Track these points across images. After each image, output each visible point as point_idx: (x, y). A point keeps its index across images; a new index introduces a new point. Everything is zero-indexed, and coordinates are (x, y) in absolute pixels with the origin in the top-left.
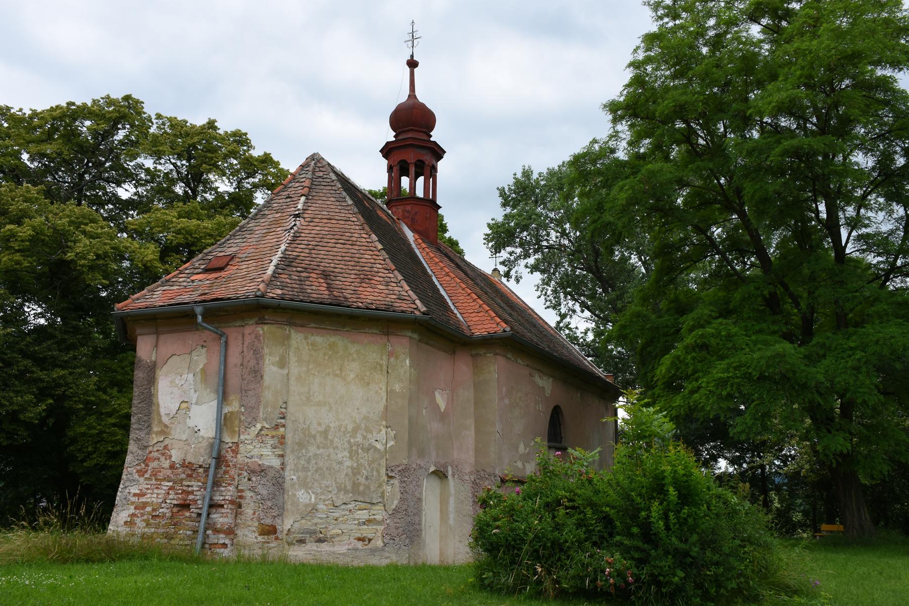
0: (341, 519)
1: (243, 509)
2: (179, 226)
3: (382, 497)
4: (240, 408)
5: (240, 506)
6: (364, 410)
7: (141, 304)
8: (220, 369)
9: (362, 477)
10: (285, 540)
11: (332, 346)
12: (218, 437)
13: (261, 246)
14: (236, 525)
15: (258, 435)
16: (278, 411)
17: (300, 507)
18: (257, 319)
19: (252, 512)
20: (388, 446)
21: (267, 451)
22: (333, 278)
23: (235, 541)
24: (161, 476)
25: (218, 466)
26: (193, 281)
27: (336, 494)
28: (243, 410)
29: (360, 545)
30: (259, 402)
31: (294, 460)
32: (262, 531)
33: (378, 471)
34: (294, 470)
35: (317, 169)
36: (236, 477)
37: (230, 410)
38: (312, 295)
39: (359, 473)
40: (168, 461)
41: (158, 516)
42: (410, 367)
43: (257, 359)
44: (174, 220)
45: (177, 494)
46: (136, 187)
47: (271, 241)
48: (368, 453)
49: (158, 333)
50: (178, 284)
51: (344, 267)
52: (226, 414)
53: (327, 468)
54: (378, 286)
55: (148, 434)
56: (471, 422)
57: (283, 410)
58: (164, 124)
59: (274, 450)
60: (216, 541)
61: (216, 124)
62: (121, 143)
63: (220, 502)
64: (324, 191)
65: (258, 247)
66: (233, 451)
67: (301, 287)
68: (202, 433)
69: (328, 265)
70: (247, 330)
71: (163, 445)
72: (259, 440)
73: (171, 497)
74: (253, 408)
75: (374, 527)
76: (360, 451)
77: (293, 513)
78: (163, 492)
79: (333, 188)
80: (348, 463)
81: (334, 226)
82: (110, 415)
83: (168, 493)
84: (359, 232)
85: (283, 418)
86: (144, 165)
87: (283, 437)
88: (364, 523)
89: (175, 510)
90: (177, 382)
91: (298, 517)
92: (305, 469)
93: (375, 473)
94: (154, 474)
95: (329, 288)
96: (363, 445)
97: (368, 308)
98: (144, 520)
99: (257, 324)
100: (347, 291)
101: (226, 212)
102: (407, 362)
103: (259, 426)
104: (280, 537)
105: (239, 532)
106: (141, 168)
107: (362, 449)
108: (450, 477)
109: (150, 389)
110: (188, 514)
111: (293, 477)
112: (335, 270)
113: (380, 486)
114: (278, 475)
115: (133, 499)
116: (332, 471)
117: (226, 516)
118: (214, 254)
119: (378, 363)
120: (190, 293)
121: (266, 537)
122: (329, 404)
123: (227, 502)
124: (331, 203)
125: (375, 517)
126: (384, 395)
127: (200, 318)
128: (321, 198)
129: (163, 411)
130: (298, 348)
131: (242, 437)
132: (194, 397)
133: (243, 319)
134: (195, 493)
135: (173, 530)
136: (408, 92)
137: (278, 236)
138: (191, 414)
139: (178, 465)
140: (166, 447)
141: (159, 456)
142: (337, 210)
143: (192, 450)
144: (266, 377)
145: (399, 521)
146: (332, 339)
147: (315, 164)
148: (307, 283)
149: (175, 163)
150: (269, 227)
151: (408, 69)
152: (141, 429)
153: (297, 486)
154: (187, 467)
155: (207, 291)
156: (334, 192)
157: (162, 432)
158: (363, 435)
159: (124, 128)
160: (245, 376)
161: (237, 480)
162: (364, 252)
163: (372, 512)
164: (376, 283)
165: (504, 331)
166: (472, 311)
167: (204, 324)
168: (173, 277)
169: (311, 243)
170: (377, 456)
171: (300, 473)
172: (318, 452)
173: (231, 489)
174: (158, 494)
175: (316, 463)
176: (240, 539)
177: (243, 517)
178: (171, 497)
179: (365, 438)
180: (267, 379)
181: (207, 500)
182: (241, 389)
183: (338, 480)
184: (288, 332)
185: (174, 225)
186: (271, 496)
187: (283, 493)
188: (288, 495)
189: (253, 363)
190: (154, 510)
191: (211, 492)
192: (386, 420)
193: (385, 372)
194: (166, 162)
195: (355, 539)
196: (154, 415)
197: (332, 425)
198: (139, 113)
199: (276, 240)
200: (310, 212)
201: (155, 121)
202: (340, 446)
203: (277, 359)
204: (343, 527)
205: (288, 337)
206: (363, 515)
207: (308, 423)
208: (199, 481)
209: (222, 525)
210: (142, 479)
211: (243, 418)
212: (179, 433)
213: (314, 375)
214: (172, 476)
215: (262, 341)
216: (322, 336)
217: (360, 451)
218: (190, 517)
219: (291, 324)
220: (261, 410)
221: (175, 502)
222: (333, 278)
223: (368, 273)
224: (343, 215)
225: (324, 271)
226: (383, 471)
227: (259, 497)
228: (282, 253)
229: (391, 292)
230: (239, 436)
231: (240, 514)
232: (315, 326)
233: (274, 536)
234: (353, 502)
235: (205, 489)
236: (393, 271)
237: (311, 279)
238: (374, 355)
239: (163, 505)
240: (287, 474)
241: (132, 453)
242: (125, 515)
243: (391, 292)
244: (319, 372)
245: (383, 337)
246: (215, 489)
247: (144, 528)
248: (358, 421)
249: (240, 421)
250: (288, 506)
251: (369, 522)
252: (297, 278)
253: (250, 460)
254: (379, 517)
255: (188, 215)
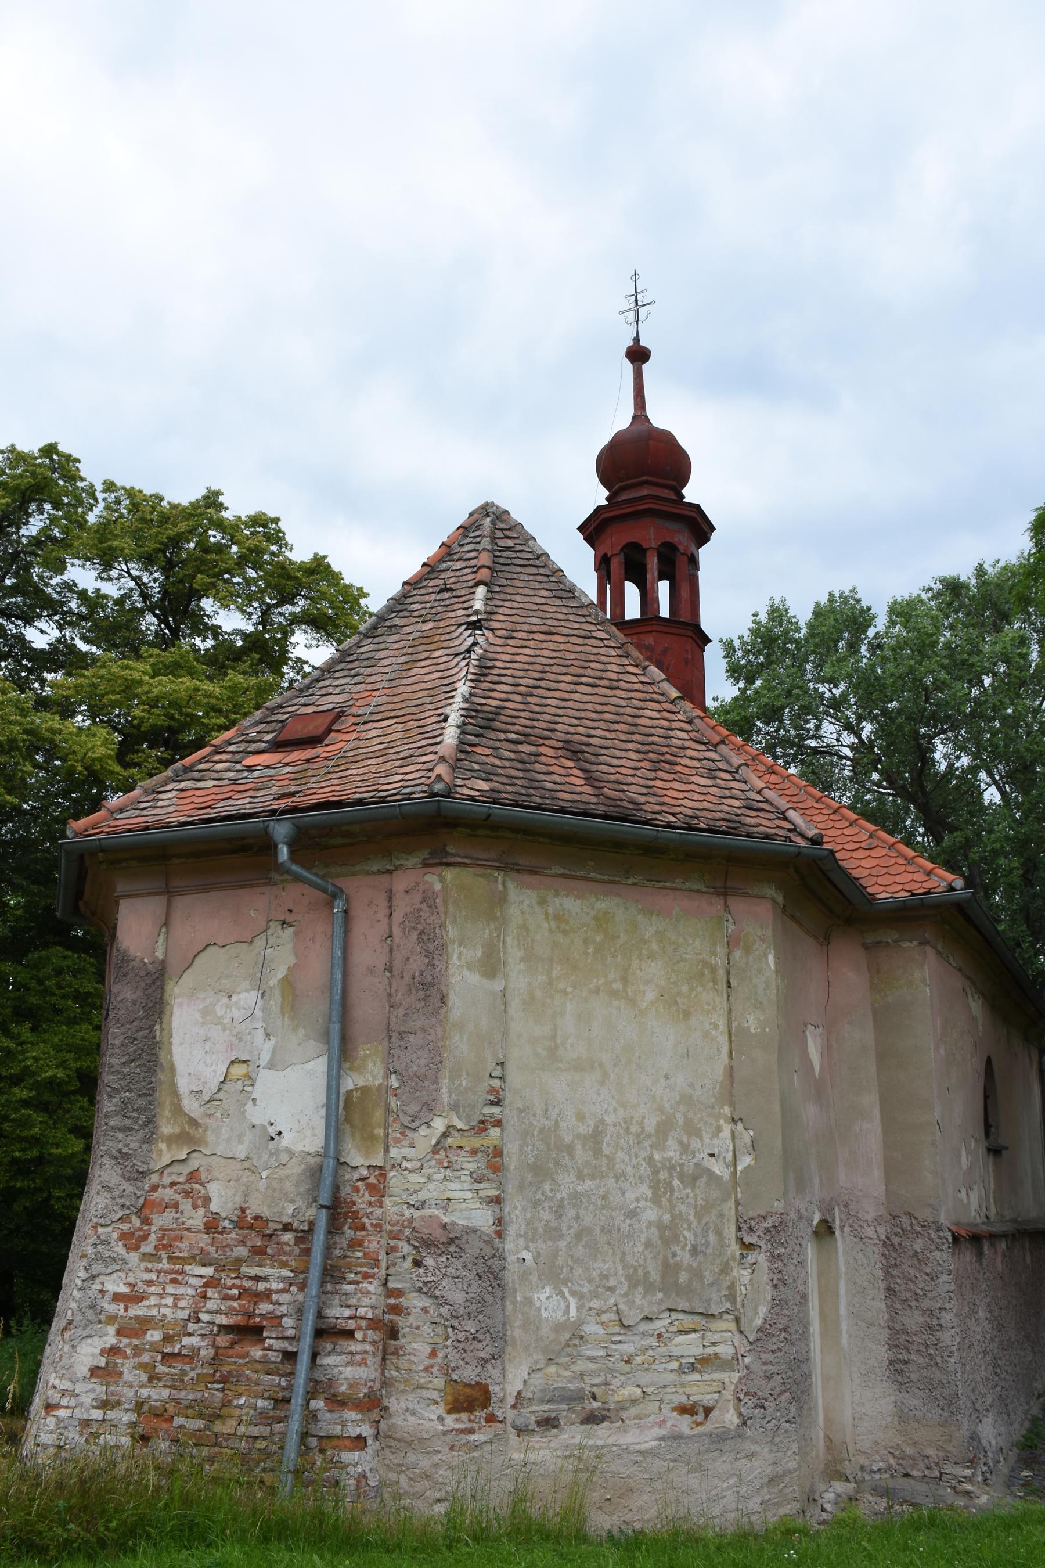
0: (638, 1359)
1: (403, 1341)
2: (156, 691)
3: (731, 1297)
4: (387, 1078)
5: (393, 1333)
6: (680, 1080)
7: (132, 819)
8: (332, 979)
9: (683, 1248)
10: (509, 1421)
11: (602, 921)
12: (332, 1152)
13: (402, 689)
14: (384, 1384)
15: (436, 1149)
16: (485, 1086)
17: (545, 1331)
18: (425, 854)
19: (428, 1349)
20: (739, 1168)
21: (459, 1189)
22: (593, 759)
23: (383, 1425)
24: (183, 1249)
25: (334, 1228)
26: (250, 768)
27: (626, 1295)
28: (394, 1082)
29: (684, 1424)
30: (437, 1062)
31: (524, 1209)
32: (456, 1400)
33: (719, 1233)
34: (525, 1236)
35: (499, 534)
36: (382, 1256)
37: (361, 1083)
38: (561, 795)
39: (676, 1239)
40: (201, 1211)
41: (179, 1354)
42: (777, 971)
43: (429, 954)
44: (146, 678)
45: (226, 1298)
46: (60, 628)
47: (427, 678)
48: (693, 1188)
49: (169, 893)
50: (216, 775)
51: (608, 735)
52: (349, 1093)
53: (603, 1229)
54: (693, 779)
55: (148, 1140)
56: (870, 1101)
57: (497, 1083)
58: (118, 502)
59: (477, 1186)
60: (337, 1430)
61: (221, 499)
62: (36, 542)
63: (342, 1324)
64: (522, 577)
65: (395, 691)
66: (371, 1188)
67: (528, 775)
68: (286, 1141)
69: (572, 730)
70: (401, 882)
71: (186, 1169)
72: (440, 1162)
73: (211, 1305)
74: (420, 1078)
75: (716, 1376)
76: (676, 1182)
77: (527, 1348)
78: (191, 1291)
79: (542, 571)
80: (651, 1214)
81: (562, 647)
82: (16, 1080)
83: (204, 1296)
84: (617, 660)
85: (497, 1103)
86: (75, 585)
87: (498, 1152)
88: (692, 1368)
89: (223, 1340)
90: (220, 1011)
91: (539, 1356)
92: (553, 1233)
93: (712, 1238)
94: (166, 1245)
95: (590, 779)
96: (682, 1165)
97: (690, 828)
98: (143, 1366)
99: (426, 865)
100: (633, 788)
101: (244, 666)
102: (771, 959)
103: (439, 1125)
104: (499, 1414)
105: (393, 1403)
106: (71, 590)
107: (682, 1177)
108: (838, 1233)
109: (151, 1028)
110: (257, 1353)
111: (525, 1255)
112: (591, 741)
113: (725, 1269)
114: (488, 1251)
115: (112, 1308)
116: (615, 1235)
117: (363, 1363)
118: (290, 709)
119: (705, 964)
120: (251, 793)
121: (464, 1416)
122: (601, 1065)
123: (364, 1323)
124: (543, 601)
125: (717, 1349)
126: (723, 1040)
127: (284, 853)
128: (520, 591)
129: (183, 1084)
130: (524, 927)
131: (394, 1152)
132: (265, 1050)
133: (387, 854)
134: (274, 1297)
135: (219, 1394)
136: (630, 412)
137: (441, 667)
138: (257, 1092)
139: (226, 1223)
140: (193, 1176)
141: (178, 1197)
142: (561, 616)
143: (262, 1185)
144: (453, 1000)
145: (770, 1357)
146: (602, 905)
147: (493, 522)
148: (538, 767)
149: (139, 578)
150: (410, 650)
151: (628, 367)
152: (131, 1129)
153: (534, 1279)
154: (251, 1227)
155: (293, 789)
156: (545, 579)
157: (182, 1138)
158: (680, 1143)
159: (41, 511)
160: (398, 998)
161: (384, 1265)
162: (640, 704)
163: (711, 1337)
164: (686, 770)
165: (952, 889)
166: (856, 846)
167: (294, 868)
168: (200, 761)
169: (521, 681)
170: (715, 1194)
171: (540, 1245)
172: (579, 1189)
173: (371, 1288)
174: (177, 1298)
175: (577, 1217)
176: (397, 1421)
177: (403, 1363)
178: (211, 1305)
179: (685, 1148)
180: (457, 1006)
181: (310, 1317)
182: (389, 1029)
183: (628, 1258)
184: (500, 887)
185: (146, 688)
186: (473, 1307)
187: (503, 1298)
188: (514, 1303)
189: (417, 963)
190: (167, 1339)
191: (318, 1297)
192: (732, 1104)
193: (722, 986)
194: (121, 576)
195: (674, 1409)
196: (163, 1095)
197: (609, 1119)
198: (73, 477)
199: (440, 674)
200: (502, 618)
201: (100, 496)
202: (629, 1171)
203: (479, 954)
204: (644, 1378)
205: (502, 899)
206: (689, 1346)
207: (553, 1114)
208: (284, 1265)
209: (351, 1386)
210: (134, 1257)
211: (394, 1103)
212: (228, 1141)
213: (564, 992)
214: (212, 1250)
215: (441, 909)
216: (578, 897)
217: (676, 1182)
218: (265, 1361)
219: (510, 867)
220: (445, 1082)
221: (224, 1320)
222: (593, 759)
223: (665, 750)
224: (577, 626)
225: (567, 742)
226: (730, 1232)
227: (444, 1310)
228: (466, 701)
229: (727, 793)
230: (387, 1150)
231: (396, 1353)
232: (561, 871)
233: (483, 1414)
234: (666, 1315)
235: (303, 1286)
236: (716, 746)
237: (543, 759)
238: (697, 943)
239: (191, 1327)
240: (509, 1246)
241: (106, 1188)
242: (90, 1350)
243: (727, 793)
244: (575, 987)
245: (714, 899)
246: (329, 1287)
247: (142, 1386)
248: (667, 1106)
249: (388, 1110)
250: (516, 1332)
251: (704, 1363)
252: (512, 755)
253: (417, 1214)
254: (725, 1350)
255: (174, 669)
